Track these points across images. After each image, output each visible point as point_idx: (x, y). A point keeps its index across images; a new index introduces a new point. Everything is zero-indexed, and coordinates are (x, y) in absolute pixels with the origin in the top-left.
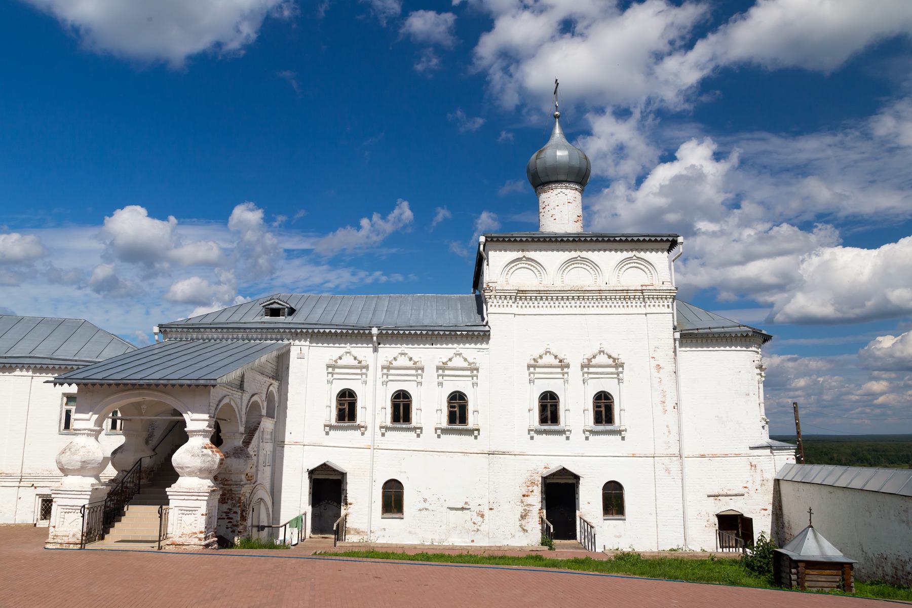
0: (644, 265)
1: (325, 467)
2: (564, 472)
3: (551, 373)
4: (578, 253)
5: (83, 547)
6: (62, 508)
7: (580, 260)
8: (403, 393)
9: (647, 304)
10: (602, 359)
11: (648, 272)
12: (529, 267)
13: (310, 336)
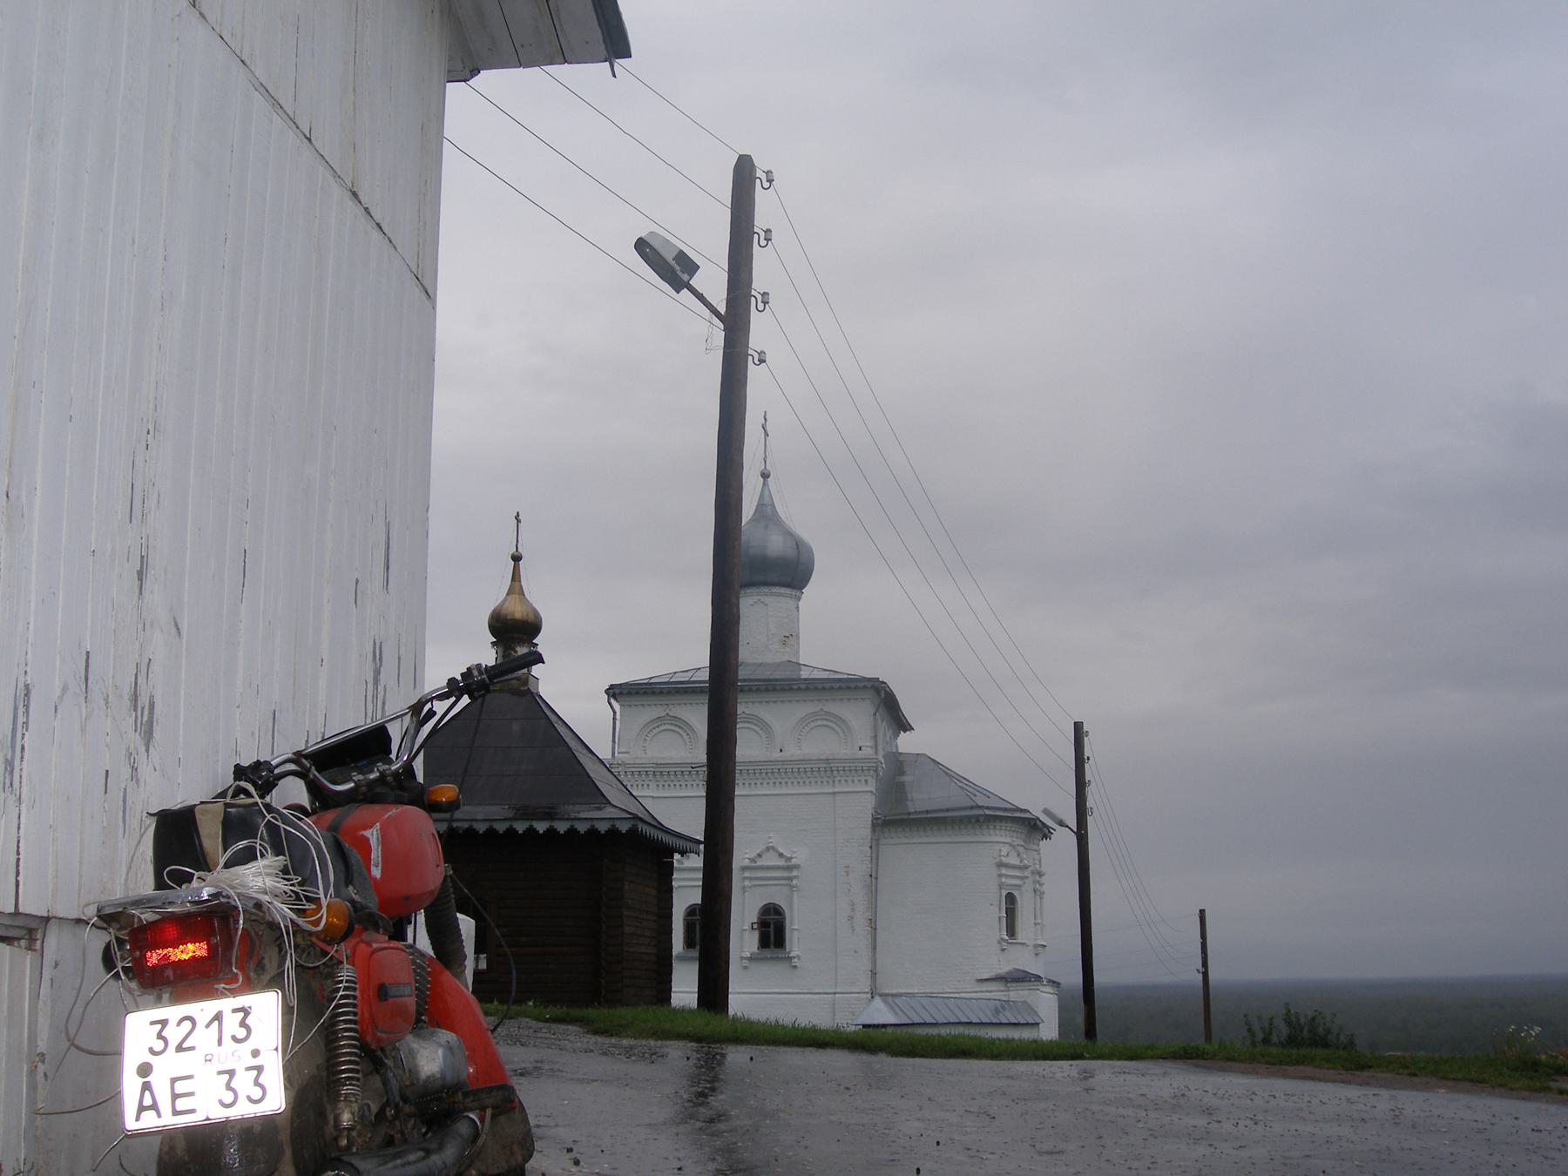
6: (192, 1111)
9: (837, 779)
10: (771, 860)
11: (841, 733)
12: (676, 729)
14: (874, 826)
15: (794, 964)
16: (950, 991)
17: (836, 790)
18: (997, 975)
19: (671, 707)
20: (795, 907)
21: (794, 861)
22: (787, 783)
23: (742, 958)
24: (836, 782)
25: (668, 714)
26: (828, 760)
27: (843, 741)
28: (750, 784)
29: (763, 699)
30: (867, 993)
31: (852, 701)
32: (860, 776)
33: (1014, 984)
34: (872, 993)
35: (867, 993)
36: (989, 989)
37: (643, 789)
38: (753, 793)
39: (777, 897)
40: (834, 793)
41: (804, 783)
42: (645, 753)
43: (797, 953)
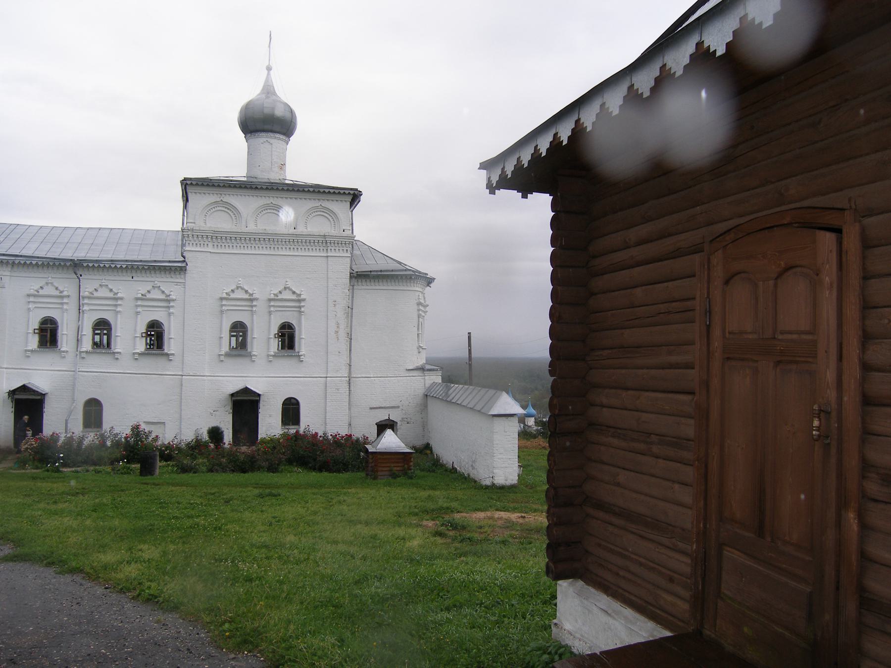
0: (327, 213)
1: (24, 388)
2: (246, 391)
3: (239, 306)
4: (271, 200)
5: (815, 415)
7: (272, 206)
8: (240, 324)
9: (329, 248)
10: (287, 295)
11: (332, 220)
12: (226, 210)
13: (11, 266)
14: (351, 277)
15: (221, 359)
16: (391, 376)
17: (329, 255)
18: (417, 367)
19: (223, 195)
20: (119, 323)
21: (302, 297)
22: (298, 249)
23: (268, 356)
24: (329, 250)
25: (222, 200)
26: (325, 236)
27: (333, 225)
28: (274, 248)
29: (343, 199)
30: (346, 377)
31: (239, 196)
32: (339, 247)
33: (428, 372)
34: (349, 377)
35: (346, 377)
36: (414, 375)
37: (204, 246)
38: (276, 253)
39: (159, 315)
40: (327, 257)
41: (309, 249)
42: (205, 224)
43: (304, 353)
